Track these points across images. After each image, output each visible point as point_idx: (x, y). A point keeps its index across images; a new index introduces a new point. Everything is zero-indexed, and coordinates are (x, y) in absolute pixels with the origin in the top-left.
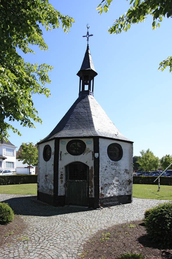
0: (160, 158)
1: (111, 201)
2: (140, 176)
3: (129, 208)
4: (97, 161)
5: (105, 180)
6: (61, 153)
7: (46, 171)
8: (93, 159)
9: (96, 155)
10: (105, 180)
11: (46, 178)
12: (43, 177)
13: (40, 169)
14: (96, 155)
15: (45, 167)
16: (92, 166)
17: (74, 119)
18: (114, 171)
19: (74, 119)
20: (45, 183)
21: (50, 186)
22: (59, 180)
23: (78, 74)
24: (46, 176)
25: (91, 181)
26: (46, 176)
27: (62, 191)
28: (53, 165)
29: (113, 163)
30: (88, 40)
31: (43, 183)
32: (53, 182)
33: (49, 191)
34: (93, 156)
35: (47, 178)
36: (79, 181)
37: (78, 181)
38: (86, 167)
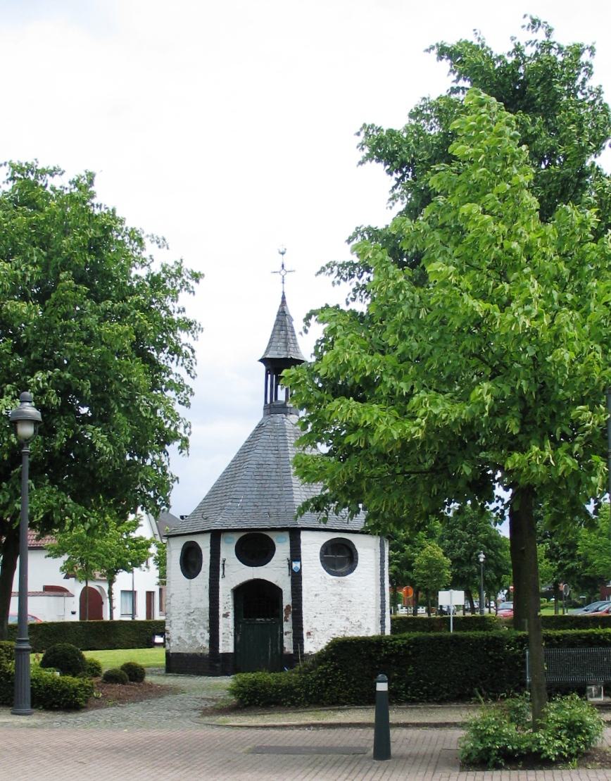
1: (183, 753)
2: (458, 149)
4: (296, 578)
6: (224, 561)
12: (181, 615)
14: (296, 565)
21: (201, 634)
22: (221, 620)
27: (227, 645)
30: (283, 282)
32: (207, 624)
38: (275, 591)
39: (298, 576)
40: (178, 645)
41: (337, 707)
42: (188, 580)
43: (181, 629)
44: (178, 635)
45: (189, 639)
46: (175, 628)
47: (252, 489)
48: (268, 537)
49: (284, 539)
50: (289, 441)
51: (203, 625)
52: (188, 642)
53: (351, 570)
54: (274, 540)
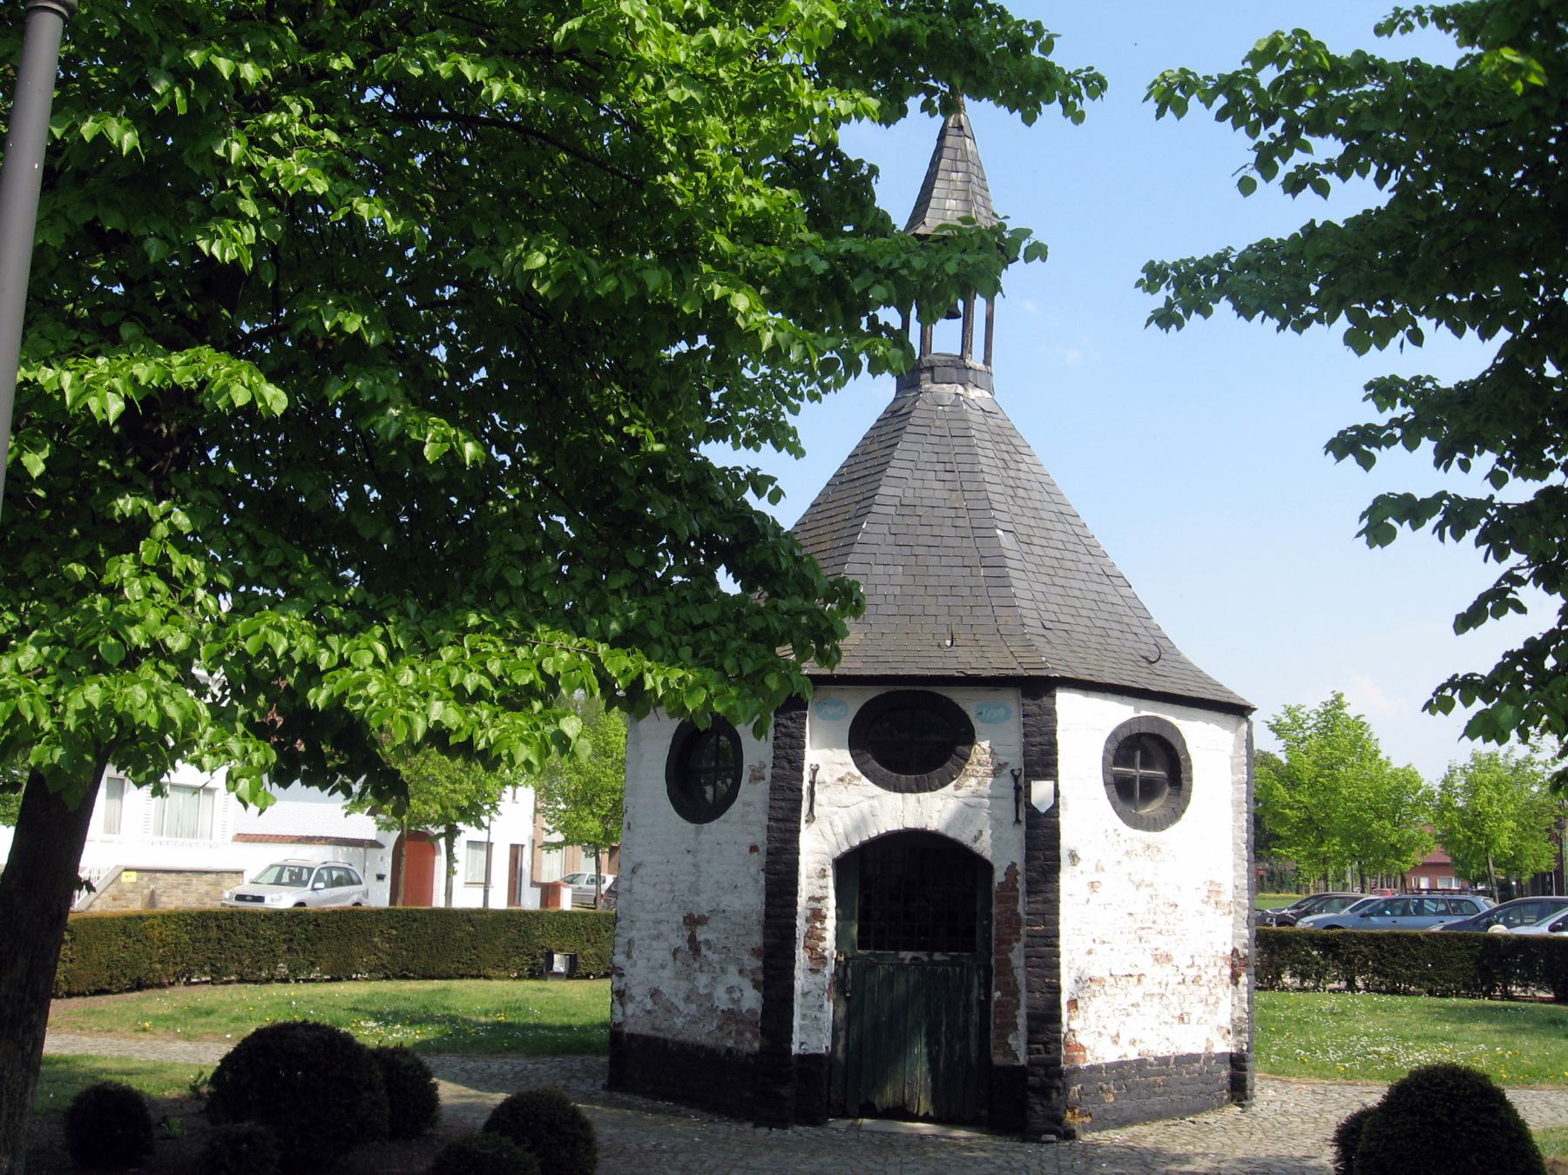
0: (1233, 736)
3: (1240, 1133)
5: (1090, 952)
6: (815, 771)
7: (695, 889)
8: (1018, 821)
9: (1041, 792)
10: (1090, 952)
11: (692, 939)
12: (664, 928)
13: (641, 871)
15: (689, 858)
16: (1014, 865)
17: (884, 549)
18: (1144, 891)
19: (884, 549)
20: (678, 975)
23: (1333, 711)
24: (693, 921)
25: (1009, 961)
26: (693, 921)
28: (754, 849)
29: (1139, 847)
31: (667, 973)
33: (720, 1028)
34: (1017, 801)
35: (702, 934)
36: (923, 956)
37: (914, 959)
39: (791, 831)
40: (649, 1012)
41: (626, 1098)
42: (692, 826)
43: (663, 967)
44: (656, 985)
45: (688, 999)
46: (642, 963)
47: (891, 570)
48: (949, 701)
49: (1002, 712)
50: (980, 451)
51: (738, 961)
52: (682, 1006)
53: (1175, 814)
54: (972, 715)
